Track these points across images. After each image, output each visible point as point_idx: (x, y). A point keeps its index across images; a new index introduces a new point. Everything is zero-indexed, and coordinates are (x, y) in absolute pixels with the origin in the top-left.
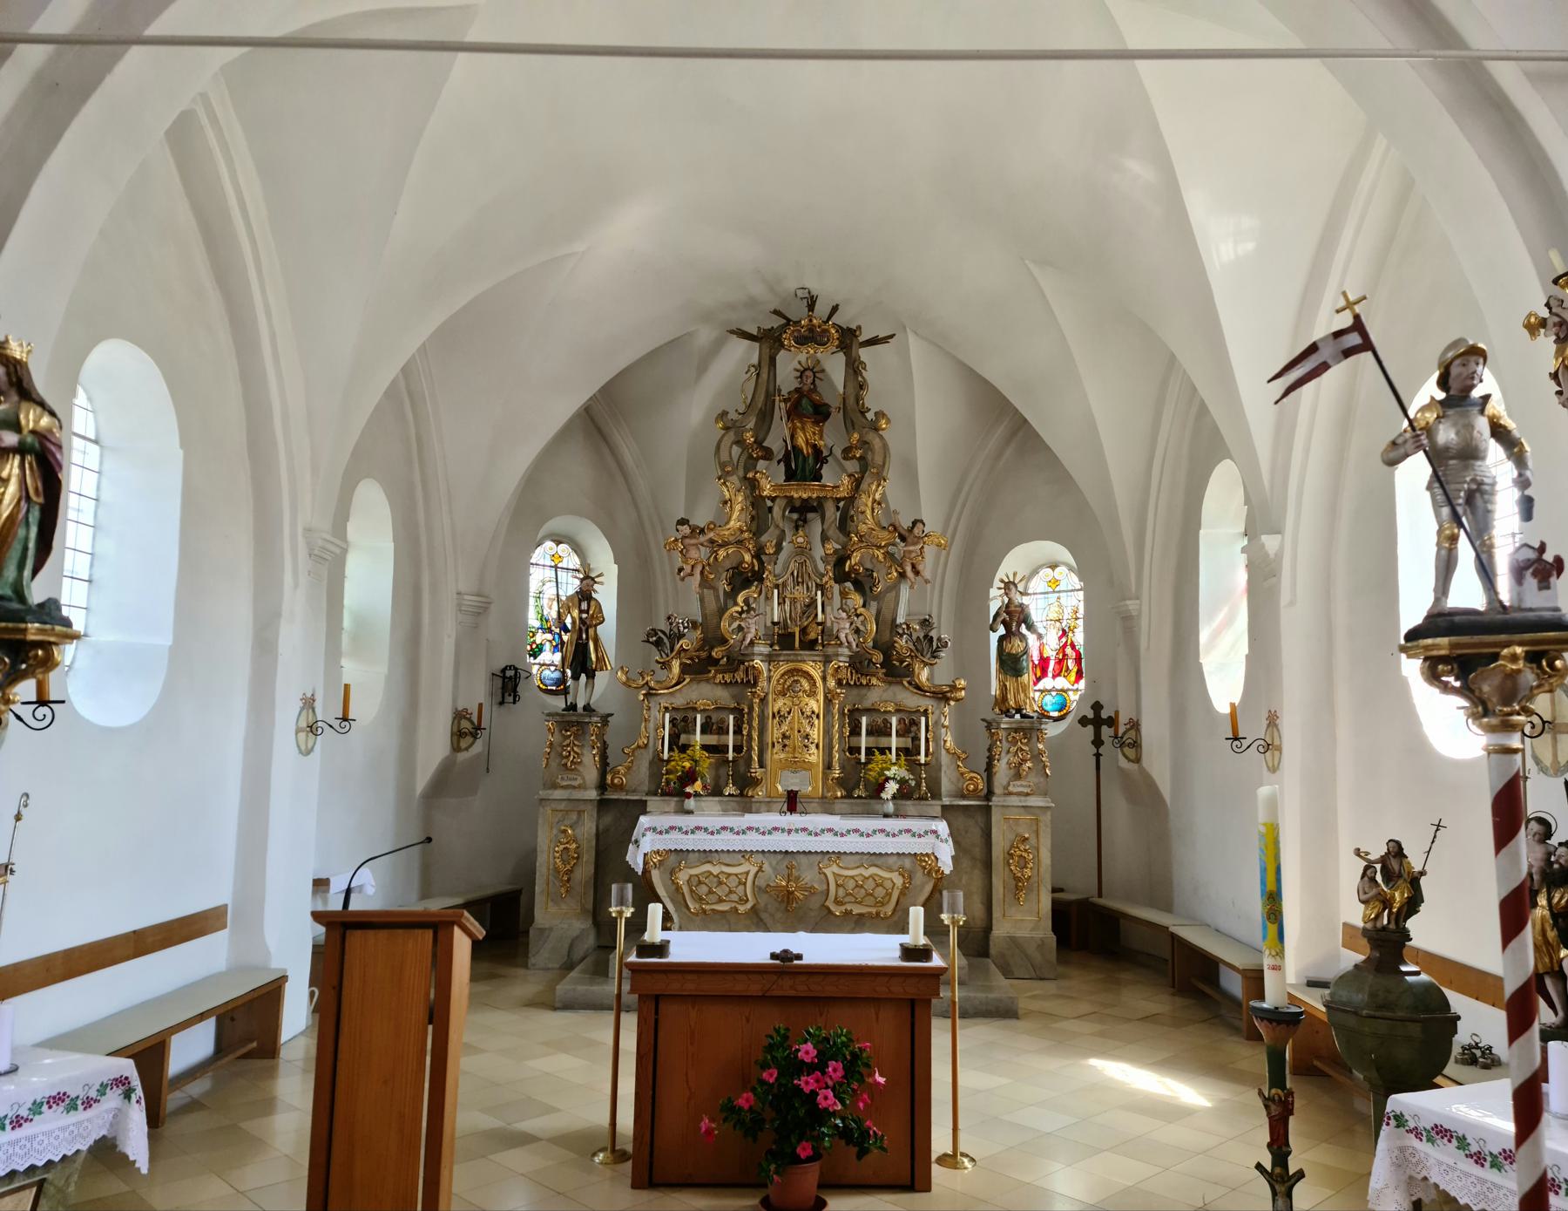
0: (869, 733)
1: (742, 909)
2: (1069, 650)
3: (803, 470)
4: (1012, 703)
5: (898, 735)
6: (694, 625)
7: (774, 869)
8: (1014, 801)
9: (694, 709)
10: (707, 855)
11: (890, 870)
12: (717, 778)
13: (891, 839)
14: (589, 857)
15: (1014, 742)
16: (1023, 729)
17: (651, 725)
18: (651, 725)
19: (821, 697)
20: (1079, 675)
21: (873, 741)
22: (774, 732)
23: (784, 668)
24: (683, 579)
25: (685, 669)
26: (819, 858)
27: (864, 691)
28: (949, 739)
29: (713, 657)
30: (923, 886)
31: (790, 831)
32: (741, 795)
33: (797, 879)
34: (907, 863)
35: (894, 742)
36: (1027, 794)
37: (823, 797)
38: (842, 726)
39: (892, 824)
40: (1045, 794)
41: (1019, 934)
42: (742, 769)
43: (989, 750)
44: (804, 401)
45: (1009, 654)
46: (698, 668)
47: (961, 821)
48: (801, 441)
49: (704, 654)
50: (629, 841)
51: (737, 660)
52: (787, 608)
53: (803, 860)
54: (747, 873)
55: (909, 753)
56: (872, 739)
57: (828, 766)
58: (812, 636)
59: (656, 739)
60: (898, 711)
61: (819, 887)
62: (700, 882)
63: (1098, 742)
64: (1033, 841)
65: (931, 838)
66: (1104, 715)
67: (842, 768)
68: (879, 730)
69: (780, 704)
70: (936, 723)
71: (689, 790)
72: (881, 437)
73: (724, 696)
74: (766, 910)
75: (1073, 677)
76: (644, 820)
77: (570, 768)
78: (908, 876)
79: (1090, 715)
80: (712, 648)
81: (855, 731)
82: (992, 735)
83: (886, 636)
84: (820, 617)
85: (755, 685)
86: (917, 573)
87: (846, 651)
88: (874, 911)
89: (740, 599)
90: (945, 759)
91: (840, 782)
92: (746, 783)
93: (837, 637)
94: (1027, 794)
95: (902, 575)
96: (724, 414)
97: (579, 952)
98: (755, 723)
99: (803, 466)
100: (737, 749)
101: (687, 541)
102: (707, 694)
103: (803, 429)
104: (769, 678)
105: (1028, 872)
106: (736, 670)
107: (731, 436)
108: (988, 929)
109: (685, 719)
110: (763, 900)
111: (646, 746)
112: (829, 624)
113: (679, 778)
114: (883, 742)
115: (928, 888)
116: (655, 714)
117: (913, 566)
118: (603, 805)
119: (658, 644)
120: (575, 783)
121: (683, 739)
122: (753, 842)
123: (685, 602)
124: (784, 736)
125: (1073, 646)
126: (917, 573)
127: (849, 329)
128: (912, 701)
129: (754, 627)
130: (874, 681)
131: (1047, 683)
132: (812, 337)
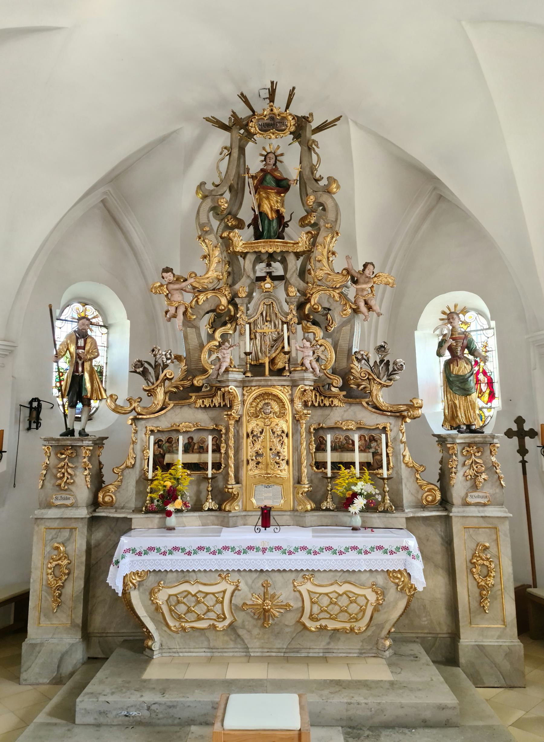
0: (334, 449)
1: (220, 626)
2: (481, 377)
3: (269, 231)
5: (361, 451)
6: (178, 358)
7: (251, 588)
8: (473, 511)
9: (178, 431)
10: (184, 576)
11: (362, 585)
12: (198, 493)
13: (363, 556)
14: (79, 572)
15: (469, 455)
16: (475, 443)
17: (138, 447)
18: (138, 447)
19: (290, 418)
20: (492, 396)
22: (248, 450)
23: (256, 392)
24: (169, 320)
25: (172, 396)
26: (293, 575)
27: (327, 411)
28: (407, 453)
29: (195, 386)
30: (396, 602)
31: (264, 550)
32: (220, 509)
33: (273, 596)
34: (380, 580)
36: (484, 505)
37: (294, 510)
38: (309, 444)
39: (363, 540)
40: (501, 504)
41: (488, 642)
42: (221, 484)
44: (269, 178)
45: (457, 376)
46: (181, 395)
47: (423, 529)
48: (266, 208)
49: (187, 383)
50: (111, 562)
51: (216, 388)
52: (258, 342)
53: (278, 577)
54: (224, 592)
56: (336, 454)
57: (299, 481)
58: (280, 365)
59: (142, 459)
60: (358, 429)
61: (295, 604)
62: (179, 602)
63: (523, 451)
64: (493, 550)
65: (402, 554)
66: (526, 428)
67: (311, 481)
69: (253, 425)
70: (395, 439)
71: (170, 508)
72: (332, 198)
73: (204, 419)
74: (243, 627)
75: (486, 397)
76: (125, 541)
77: (63, 486)
78: (382, 593)
79: (515, 428)
80: (194, 377)
81: (321, 447)
83: (343, 364)
84: (287, 349)
85: (231, 408)
86: (370, 308)
87: (310, 376)
88: (348, 626)
89: (218, 335)
90: (405, 472)
91: (310, 495)
92: (223, 498)
93: (302, 364)
94: (484, 505)
95: (356, 311)
96: (203, 184)
97: (67, 668)
98: (231, 443)
99: (268, 227)
100: (217, 466)
101: (171, 286)
102: (189, 417)
103: (268, 198)
104: (243, 402)
105: (491, 581)
106: (214, 395)
107: (208, 203)
108: (455, 636)
109: (169, 441)
110: (241, 617)
111: (134, 466)
112: (293, 354)
113: (162, 496)
114: (346, 457)
115: (402, 604)
116: (141, 435)
117: (366, 303)
118: (93, 521)
119: (144, 373)
120: (68, 502)
121: (168, 458)
122: (229, 561)
123: (173, 340)
124: (258, 454)
125: (485, 373)
126: (370, 308)
127: (304, 117)
128: (372, 420)
129: (229, 356)
130: (336, 402)
132: (273, 124)
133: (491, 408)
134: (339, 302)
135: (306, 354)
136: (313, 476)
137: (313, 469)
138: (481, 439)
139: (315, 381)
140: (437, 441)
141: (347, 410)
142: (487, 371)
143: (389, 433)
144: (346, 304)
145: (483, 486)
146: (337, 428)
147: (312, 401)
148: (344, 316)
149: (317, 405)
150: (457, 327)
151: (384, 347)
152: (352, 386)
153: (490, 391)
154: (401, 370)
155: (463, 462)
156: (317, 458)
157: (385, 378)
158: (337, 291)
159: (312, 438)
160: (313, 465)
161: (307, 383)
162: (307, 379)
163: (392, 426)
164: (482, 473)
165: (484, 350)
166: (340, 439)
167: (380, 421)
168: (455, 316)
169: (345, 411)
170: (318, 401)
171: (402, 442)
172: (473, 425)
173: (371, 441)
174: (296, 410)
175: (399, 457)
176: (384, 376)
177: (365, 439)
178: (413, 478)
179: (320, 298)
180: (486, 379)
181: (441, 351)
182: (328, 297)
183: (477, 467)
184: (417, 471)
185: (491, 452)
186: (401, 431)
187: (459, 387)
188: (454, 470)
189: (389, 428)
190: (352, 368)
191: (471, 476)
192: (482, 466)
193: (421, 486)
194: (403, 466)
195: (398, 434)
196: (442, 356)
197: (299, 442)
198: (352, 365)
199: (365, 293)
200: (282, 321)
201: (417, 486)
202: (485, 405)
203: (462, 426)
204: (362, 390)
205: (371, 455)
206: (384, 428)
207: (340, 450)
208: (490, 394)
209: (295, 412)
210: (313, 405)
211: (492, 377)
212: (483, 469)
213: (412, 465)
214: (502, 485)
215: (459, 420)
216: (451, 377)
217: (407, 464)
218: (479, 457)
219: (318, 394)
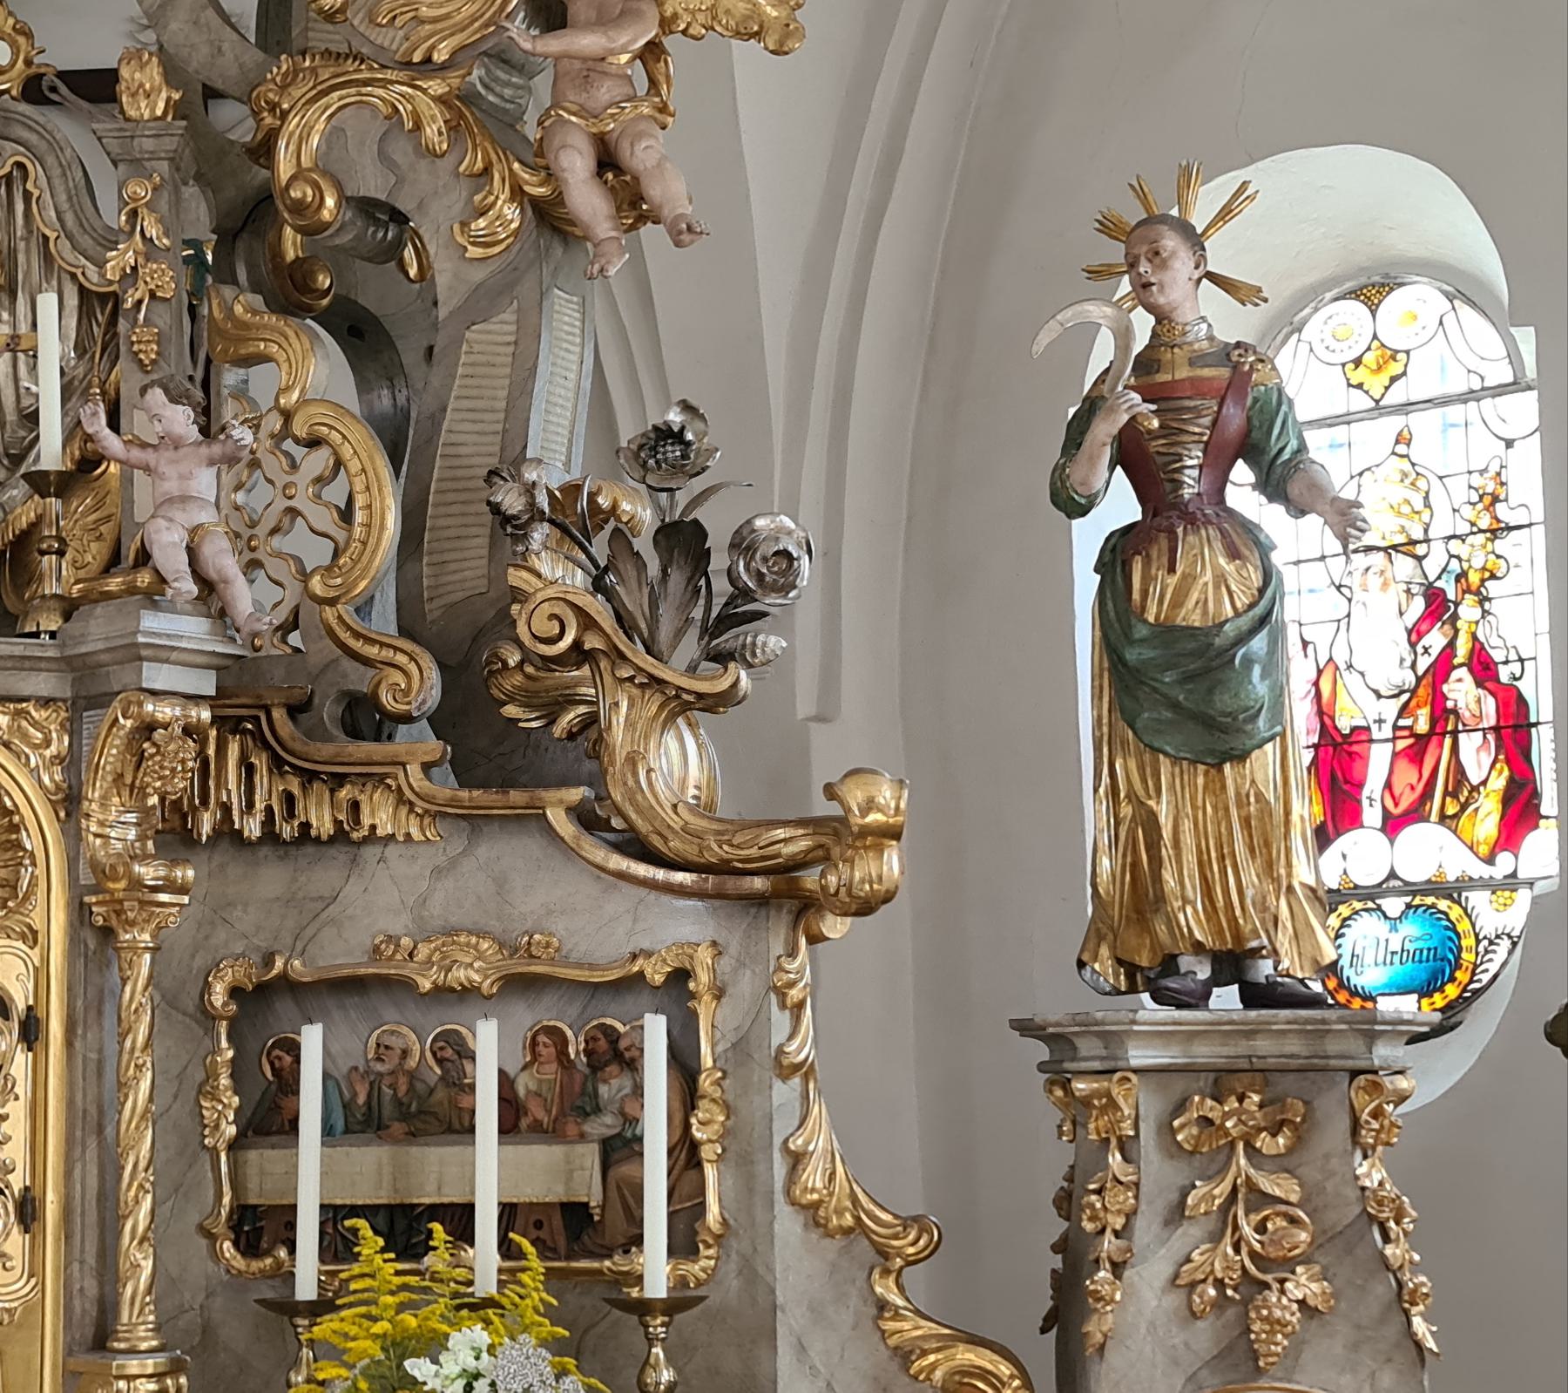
2: (1462, 690)
4: (1192, 920)
15: (1212, 1152)
16: (1261, 1074)
20: (1520, 811)
21: (372, 1172)
27: (323, 875)
28: (819, 1139)
35: (489, 1171)
43: (1067, 1203)
45: (1167, 632)
48: (445, 146)
55: (575, 1233)
60: (520, 985)
68: (407, 1107)
70: (740, 1049)
75: (1487, 819)
81: (269, 1120)
82: (1078, 1111)
83: (463, 566)
86: (633, 203)
90: (795, 1262)
114: (429, 1173)
117: (607, 161)
125: (1483, 668)
131: (1362, 855)
133: (1512, 882)
134: (450, 160)
135: (171, 486)
136: (218, 1302)
137: (216, 1256)
138: (1294, 1046)
139: (224, 667)
140: (1042, 1067)
141: (453, 863)
142: (1498, 656)
143: (705, 1010)
144: (487, 171)
145: (1294, 1353)
146: (385, 982)
147: (226, 809)
148: (474, 252)
149: (253, 828)
150: (1185, 315)
151: (678, 437)
152: (511, 711)
153: (1511, 781)
154: (785, 589)
155: (1174, 1196)
156: (253, 1184)
157: (690, 647)
158: (436, 87)
159: (216, 1050)
160: (221, 1228)
161: (157, 676)
162: (164, 654)
163: (726, 963)
164: (1289, 1264)
165: (1485, 522)
166: (405, 1053)
167: (678, 929)
168: (1171, 242)
169: (437, 872)
170: (260, 805)
171: (786, 1070)
172: (1256, 953)
173: (596, 1064)
174: (95, 865)
175: (760, 1168)
176: (679, 634)
177: (562, 1053)
178: (854, 1301)
179: (334, 136)
180: (1490, 705)
181: (1076, 473)
182: (380, 127)
183: (1261, 1228)
184: (884, 1253)
185: (1356, 1126)
186: (782, 994)
187: (1175, 706)
188: (1109, 1244)
189: (704, 977)
190: (518, 595)
191: (1220, 1284)
192: (1294, 1221)
193: (904, 1355)
194: (787, 1223)
195: (759, 1018)
196: (1084, 511)
197: (110, 1076)
198: (517, 577)
199: (605, 92)
200: (82, 291)
201: (885, 1353)
202: (1479, 870)
203: (1186, 962)
204: (571, 736)
205: (589, 1156)
206: (681, 976)
207: (398, 1128)
208: (1507, 799)
209: (87, 878)
210: (227, 833)
211: (1526, 687)
212: (1304, 1236)
213: (848, 1220)
214: (1419, 1346)
215: (1171, 923)
216: (1132, 642)
217: (812, 1213)
218: (1282, 1164)
219: (260, 761)
